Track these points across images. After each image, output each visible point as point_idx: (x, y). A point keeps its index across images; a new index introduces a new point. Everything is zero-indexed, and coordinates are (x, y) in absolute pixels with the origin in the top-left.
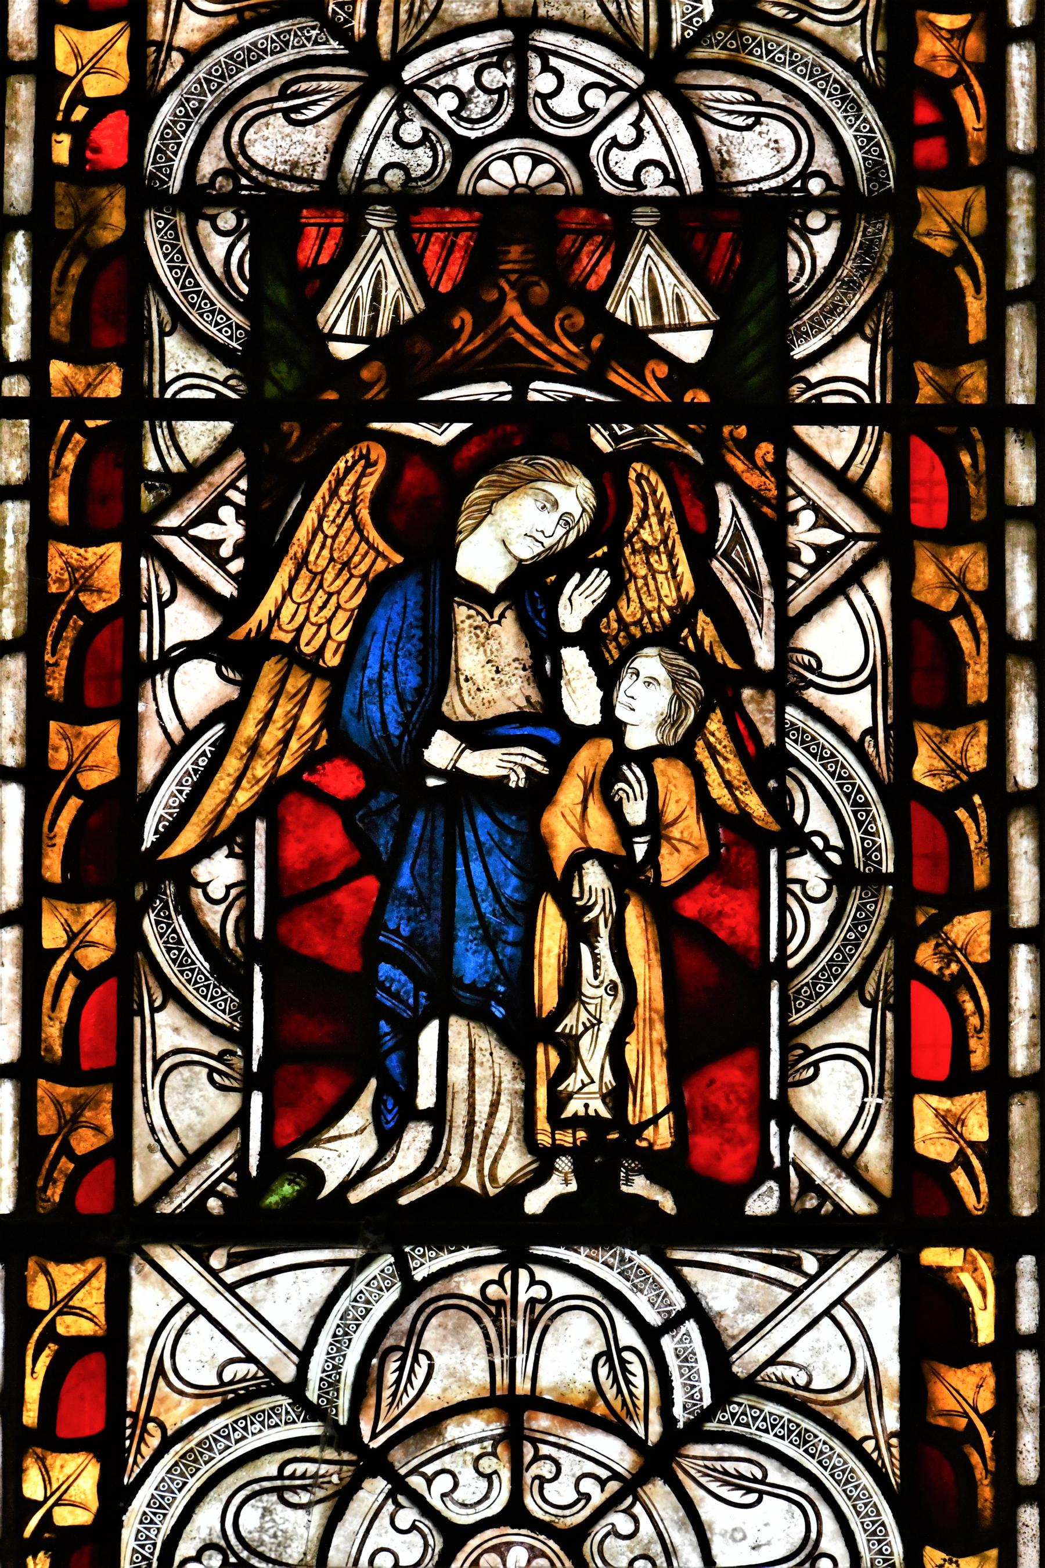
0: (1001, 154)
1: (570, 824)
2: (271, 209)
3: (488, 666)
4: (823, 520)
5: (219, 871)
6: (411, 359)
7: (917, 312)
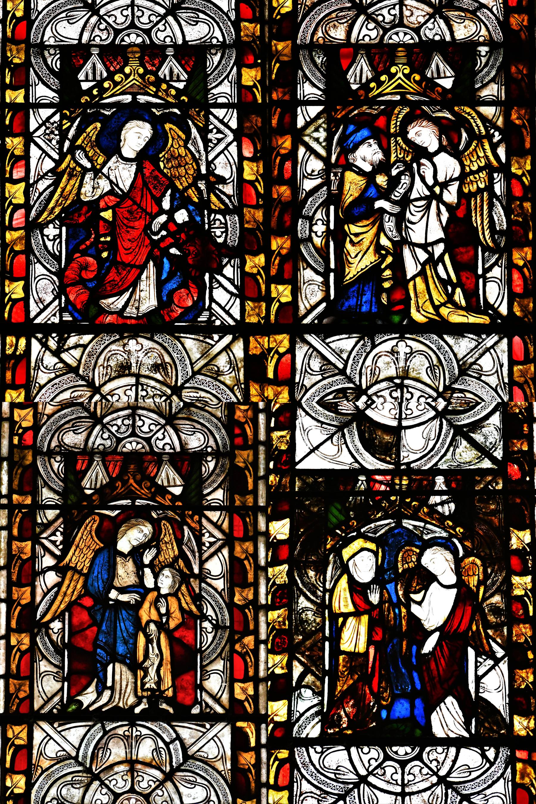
0: (257, 442)
1: (146, 613)
2: (332, 50)
3: (125, 573)
4: (211, 535)
5: (56, 625)
6: (105, 494)
7: (235, 482)
